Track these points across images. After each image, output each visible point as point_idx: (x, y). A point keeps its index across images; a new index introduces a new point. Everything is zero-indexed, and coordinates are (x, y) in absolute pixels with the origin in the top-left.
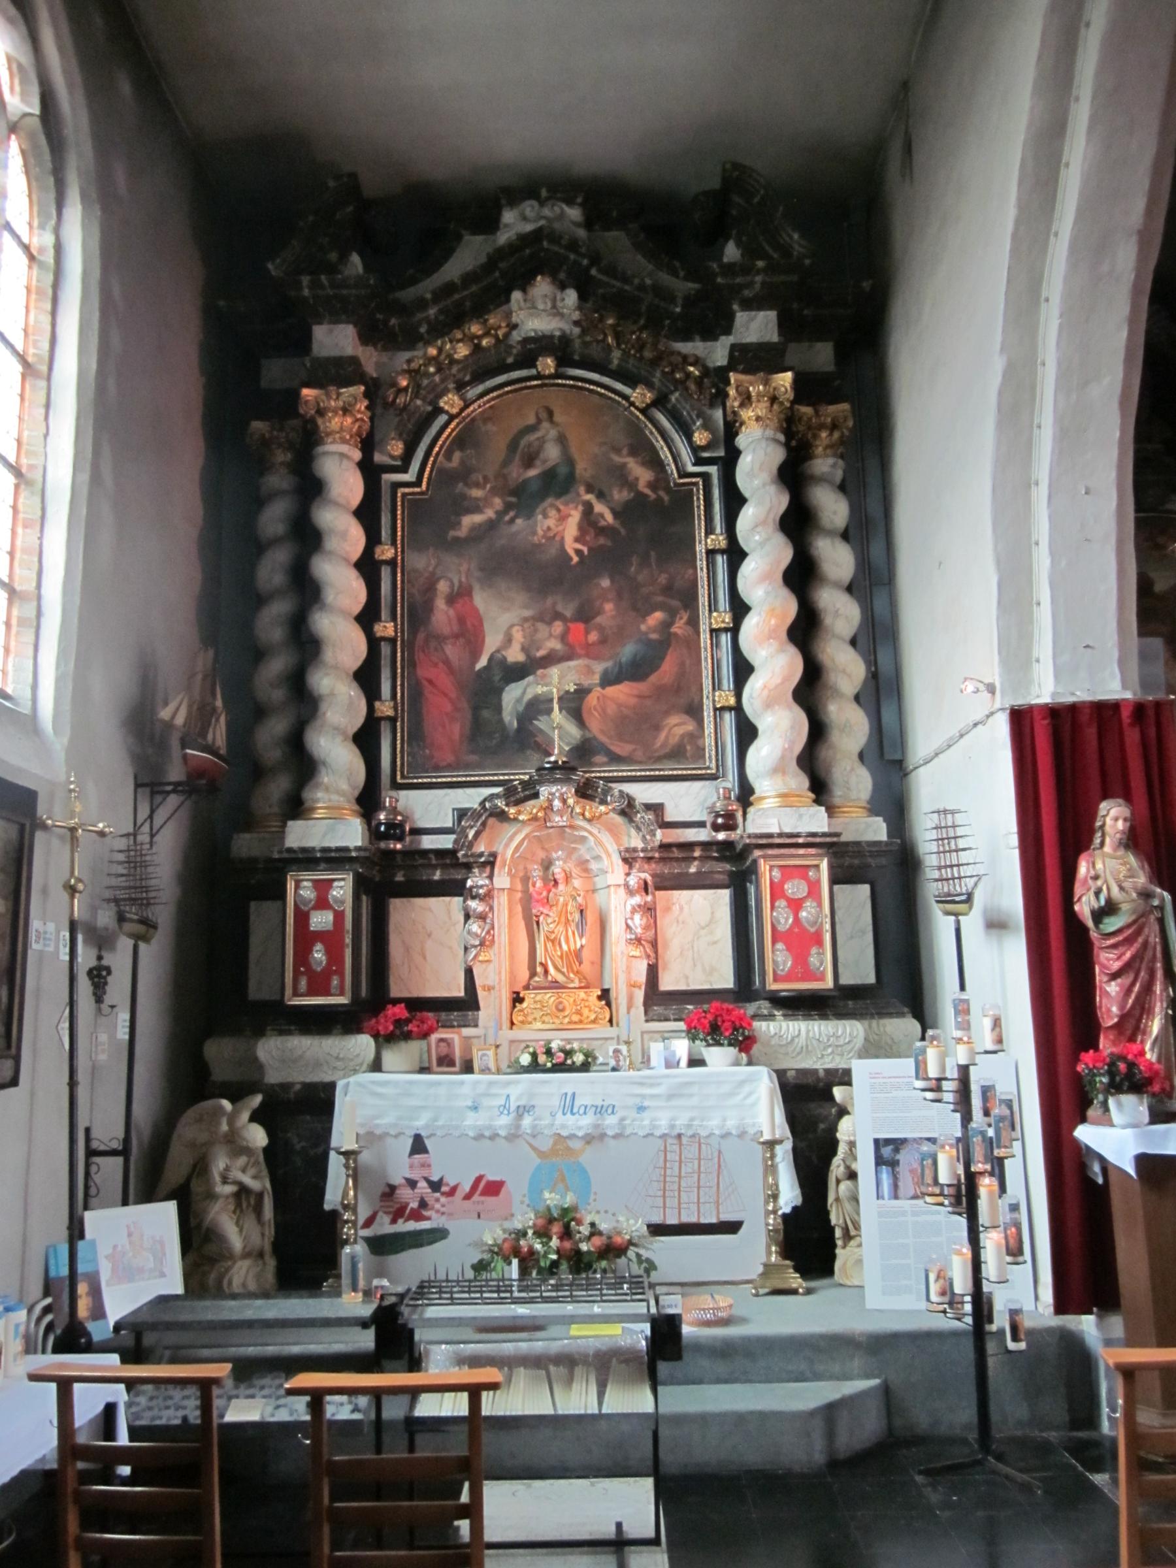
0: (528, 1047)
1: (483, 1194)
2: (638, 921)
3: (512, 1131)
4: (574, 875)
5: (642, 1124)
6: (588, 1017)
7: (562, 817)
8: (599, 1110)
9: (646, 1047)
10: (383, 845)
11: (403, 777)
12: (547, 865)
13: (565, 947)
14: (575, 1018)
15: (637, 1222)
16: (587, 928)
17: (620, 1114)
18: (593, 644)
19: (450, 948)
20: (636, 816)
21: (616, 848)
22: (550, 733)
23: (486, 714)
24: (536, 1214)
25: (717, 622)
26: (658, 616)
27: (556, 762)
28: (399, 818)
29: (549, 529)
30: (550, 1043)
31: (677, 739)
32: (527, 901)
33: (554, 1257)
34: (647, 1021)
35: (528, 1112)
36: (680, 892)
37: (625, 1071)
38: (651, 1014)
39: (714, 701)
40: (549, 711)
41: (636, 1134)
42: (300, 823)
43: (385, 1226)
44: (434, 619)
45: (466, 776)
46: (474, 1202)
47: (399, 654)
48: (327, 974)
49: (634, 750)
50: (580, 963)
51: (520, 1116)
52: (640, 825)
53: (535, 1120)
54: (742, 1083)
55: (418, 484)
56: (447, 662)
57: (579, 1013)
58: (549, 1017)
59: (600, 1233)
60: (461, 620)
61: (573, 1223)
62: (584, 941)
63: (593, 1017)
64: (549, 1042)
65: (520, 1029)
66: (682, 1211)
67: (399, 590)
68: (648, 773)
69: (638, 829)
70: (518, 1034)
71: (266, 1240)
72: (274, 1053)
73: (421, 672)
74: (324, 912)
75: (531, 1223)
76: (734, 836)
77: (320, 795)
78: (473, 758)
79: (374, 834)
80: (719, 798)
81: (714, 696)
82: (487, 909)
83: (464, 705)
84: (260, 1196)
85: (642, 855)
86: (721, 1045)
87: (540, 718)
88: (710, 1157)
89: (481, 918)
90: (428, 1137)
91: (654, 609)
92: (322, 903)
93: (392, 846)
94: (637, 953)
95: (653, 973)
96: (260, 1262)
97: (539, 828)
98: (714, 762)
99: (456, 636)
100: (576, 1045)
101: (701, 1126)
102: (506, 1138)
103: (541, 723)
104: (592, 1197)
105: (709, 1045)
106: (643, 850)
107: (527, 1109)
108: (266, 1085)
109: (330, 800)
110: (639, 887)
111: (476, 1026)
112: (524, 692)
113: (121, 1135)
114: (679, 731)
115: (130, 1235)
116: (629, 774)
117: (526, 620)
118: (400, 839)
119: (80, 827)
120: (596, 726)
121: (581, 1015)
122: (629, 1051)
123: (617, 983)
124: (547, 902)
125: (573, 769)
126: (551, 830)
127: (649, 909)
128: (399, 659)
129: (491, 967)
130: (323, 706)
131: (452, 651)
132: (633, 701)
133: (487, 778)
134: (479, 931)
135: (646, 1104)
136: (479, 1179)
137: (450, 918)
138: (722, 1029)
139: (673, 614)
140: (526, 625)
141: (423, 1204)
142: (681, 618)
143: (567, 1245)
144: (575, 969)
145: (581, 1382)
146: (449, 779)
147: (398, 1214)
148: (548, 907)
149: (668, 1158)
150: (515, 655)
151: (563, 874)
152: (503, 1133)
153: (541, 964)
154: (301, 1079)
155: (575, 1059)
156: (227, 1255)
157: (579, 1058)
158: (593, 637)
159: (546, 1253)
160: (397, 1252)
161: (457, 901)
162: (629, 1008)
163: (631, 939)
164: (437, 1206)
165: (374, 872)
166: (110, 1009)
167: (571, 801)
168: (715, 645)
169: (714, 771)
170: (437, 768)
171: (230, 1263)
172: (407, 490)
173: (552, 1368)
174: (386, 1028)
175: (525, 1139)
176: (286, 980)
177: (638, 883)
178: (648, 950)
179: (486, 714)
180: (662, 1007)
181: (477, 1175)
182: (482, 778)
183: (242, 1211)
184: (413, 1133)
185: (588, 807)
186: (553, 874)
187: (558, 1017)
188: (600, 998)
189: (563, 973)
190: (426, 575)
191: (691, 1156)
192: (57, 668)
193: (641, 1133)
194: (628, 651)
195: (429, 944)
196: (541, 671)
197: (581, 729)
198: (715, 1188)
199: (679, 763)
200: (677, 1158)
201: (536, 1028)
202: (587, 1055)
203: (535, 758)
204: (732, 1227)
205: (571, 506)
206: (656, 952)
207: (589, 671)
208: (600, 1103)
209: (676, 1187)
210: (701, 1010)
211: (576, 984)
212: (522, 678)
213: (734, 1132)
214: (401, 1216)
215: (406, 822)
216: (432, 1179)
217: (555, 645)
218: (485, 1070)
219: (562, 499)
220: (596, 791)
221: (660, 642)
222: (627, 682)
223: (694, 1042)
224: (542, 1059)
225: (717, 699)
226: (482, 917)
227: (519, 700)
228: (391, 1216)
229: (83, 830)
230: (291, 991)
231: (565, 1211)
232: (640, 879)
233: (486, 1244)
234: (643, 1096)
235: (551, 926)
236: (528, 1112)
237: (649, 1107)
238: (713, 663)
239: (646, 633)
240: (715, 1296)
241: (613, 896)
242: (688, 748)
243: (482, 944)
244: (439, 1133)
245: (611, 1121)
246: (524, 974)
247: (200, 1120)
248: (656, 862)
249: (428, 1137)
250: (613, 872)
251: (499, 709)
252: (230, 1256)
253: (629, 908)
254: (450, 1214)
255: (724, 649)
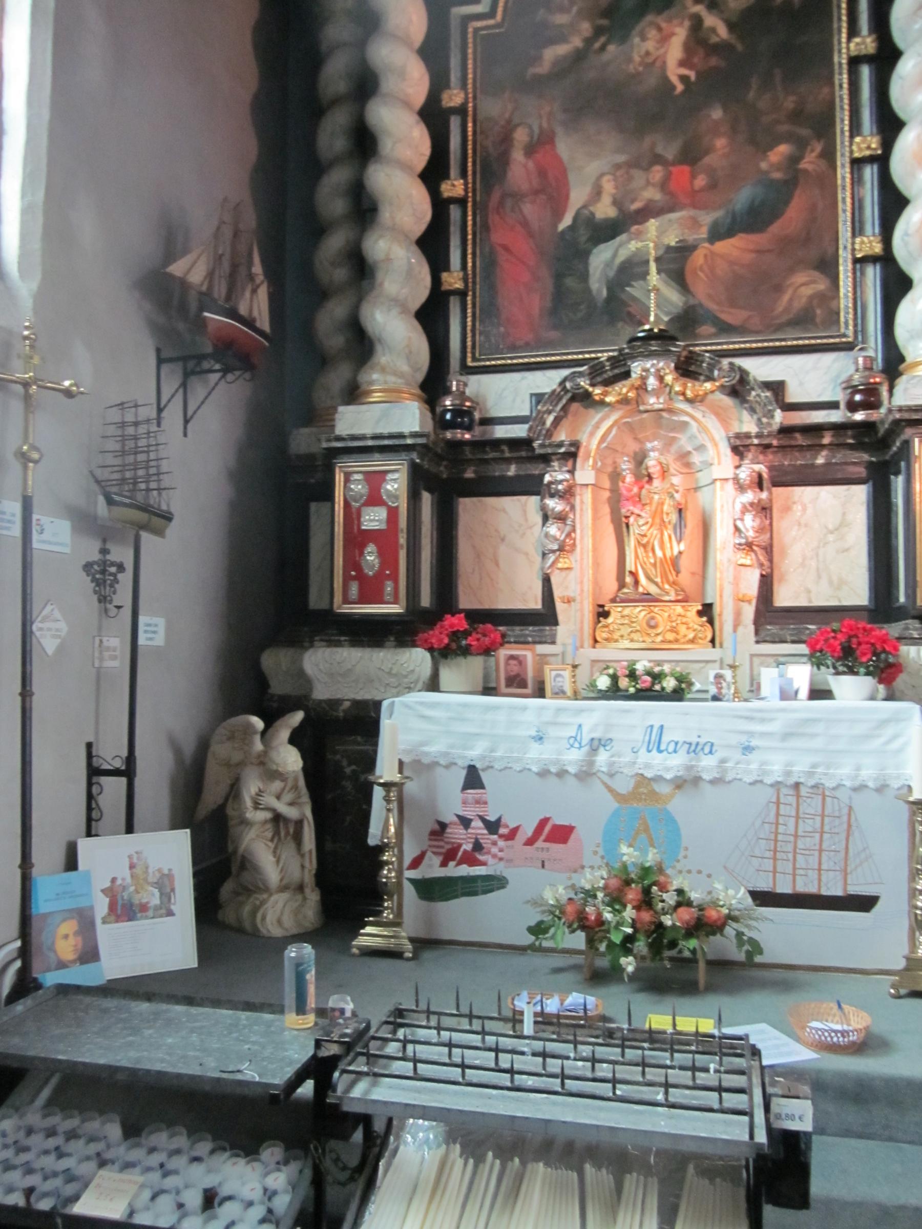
0: (608, 668)
1: (549, 839)
2: (750, 523)
3: (584, 769)
4: (672, 471)
5: (751, 767)
6: (685, 636)
7: (658, 398)
8: (693, 748)
9: (755, 673)
10: (449, 435)
11: (474, 359)
12: (640, 459)
13: (659, 553)
14: (670, 636)
15: (737, 892)
16: (688, 531)
17: (719, 755)
18: (702, 190)
19: (527, 554)
20: (750, 393)
21: (723, 434)
22: (643, 299)
23: (570, 282)
24: (609, 872)
25: (860, 150)
26: (783, 149)
27: (651, 330)
28: (468, 404)
29: (648, 53)
30: (634, 664)
31: (804, 300)
32: (616, 501)
33: (629, 930)
34: (757, 642)
35: (604, 746)
36: (802, 488)
37: (727, 701)
38: (763, 634)
39: (853, 250)
40: (644, 275)
41: (740, 780)
42: (351, 408)
43: (433, 869)
44: (510, 174)
45: (547, 355)
46: (538, 848)
47: (470, 218)
48: (380, 577)
49: (750, 317)
50: (678, 572)
51: (594, 751)
52: (754, 405)
53: (612, 756)
54: (884, 723)
55: (492, 14)
56: (525, 224)
57: (674, 630)
58: (638, 634)
59: (689, 904)
60: (542, 173)
61: (655, 888)
62: (682, 547)
63: (691, 635)
64: (634, 662)
65: (604, 647)
66: (798, 878)
67: (470, 143)
68: (766, 344)
69: (752, 410)
70: (604, 653)
71: (306, 871)
72: (322, 667)
73: (497, 237)
74: (376, 509)
75: (602, 883)
76: (874, 415)
77: (375, 376)
78: (553, 334)
79: (441, 424)
80: (857, 370)
81: (853, 244)
82: (568, 509)
83: (545, 274)
84: (299, 823)
85: (756, 441)
86: (856, 674)
87: (634, 283)
88: (837, 814)
89: (560, 519)
90: (483, 770)
91: (778, 140)
92: (374, 499)
93: (459, 436)
94: (748, 562)
95: (767, 584)
96: (299, 897)
97: (630, 414)
98: (851, 328)
99: (536, 192)
100: (666, 668)
101: (825, 774)
102: (576, 776)
103: (634, 290)
104: (682, 853)
105: (838, 673)
106: (759, 436)
107: (603, 743)
108: (314, 700)
109: (386, 382)
110: (751, 482)
111: (553, 643)
112: (615, 255)
113: (125, 753)
114: (807, 291)
115: (132, 867)
116: (743, 346)
117: (618, 166)
118: (469, 428)
119: (35, 383)
120: (702, 291)
121: (677, 633)
122: (734, 677)
123: (721, 596)
124: (638, 500)
125: (673, 339)
126: (645, 415)
127: (764, 509)
128: (470, 223)
129: (572, 575)
130: (380, 275)
131: (529, 209)
132: (749, 257)
133: (570, 357)
134: (558, 534)
135: (754, 743)
136: (544, 822)
137: (526, 520)
138: (858, 652)
139: (802, 145)
140: (618, 173)
141: (478, 846)
142: (812, 151)
143: (646, 916)
144: (671, 579)
145: (634, 1211)
146: (526, 360)
147: (449, 856)
148: (639, 506)
149: (782, 812)
150: (605, 210)
151: (658, 468)
152: (572, 769)
153: (631, 572)
154: (352, 696)
155: (665, 684)
156: (261, 886)
157: (670, 684)
158: (701, 181)
159: (619, 924)
160: (447, 899)
161: (534, 500)
162: (736, 626)
163: (740, 544)
164: (494, 850)
165: (442, 468)
166: (116, 610)
167: (669, 379)
168: (857, 181)
169: (850, 340)
170: (513, 348)
171: (265, 896)
172: (479, 24)
173: (588, 1168)
174: (441, 640)
175: (599, 778)
176: (335, 586)
177: (750, 476)
178: (761, 558)
179: (570, 282)
180: (777, 627)
181: (542, 817)
182: (565, 357)
183: (280, 839)
184: (467, 764)
185: (689, 385)
186: (647, 468)
187: (648, 634)
188: (700, 613)
189: (656, 584)
190: (503, 123)
191: (813, 812)
192: (23, 196)
193: (748, 779)
194: (743, 197)
195: (503, 549)
196: (636, 227)
197: (683, 295)
198: (843, 854)
199: (807, 330)
200: (793, 813)
201: (622, 647)
202: (680, 679)
203: (627, 332)
204: (865, 903)
205: (675, 22)
206: (771, 560)
207: (695, 223)
208: (694, 740)
209: (790, 848)
210: (829, 630)
211: (672, 597)
212: (613, 237)
213: (871, 784)
214: (453, 859)
215: (475, 408)
216: (488, 818)
217: (653, 194)
218: (560, 693)
219: (666, 14)
220: (701, 366)
221: (786, 182)
222: (741, 235)
223: (819, 668)
224: (624, 683)
225: (857, 247)
226: (561, 518)
227: (608, 265)
228: (441, 858)
229: (39, 386)
230: (341, 598)
231: (646, 871)
232: (754, 471)
233: (547, 904)
234: (751, 734)
235: (644, 528)
236: (604, 746)
237: (758, 747)
238: (853, 204)
239: (767, 172)
240: (843, 1006)
241: (719, 493)
242: (818, 312)
243: (561, 549)
244: (497, 766)
245: (707, 764)
246: (611, 586)
247: (231, 738)
248: (774, 453)
249: (483, 770)
250: (719, 463)
251: (584, 277)
252: (267, 889)
253: (738, 507)
254: (510, 861)
255: (868, 185)
